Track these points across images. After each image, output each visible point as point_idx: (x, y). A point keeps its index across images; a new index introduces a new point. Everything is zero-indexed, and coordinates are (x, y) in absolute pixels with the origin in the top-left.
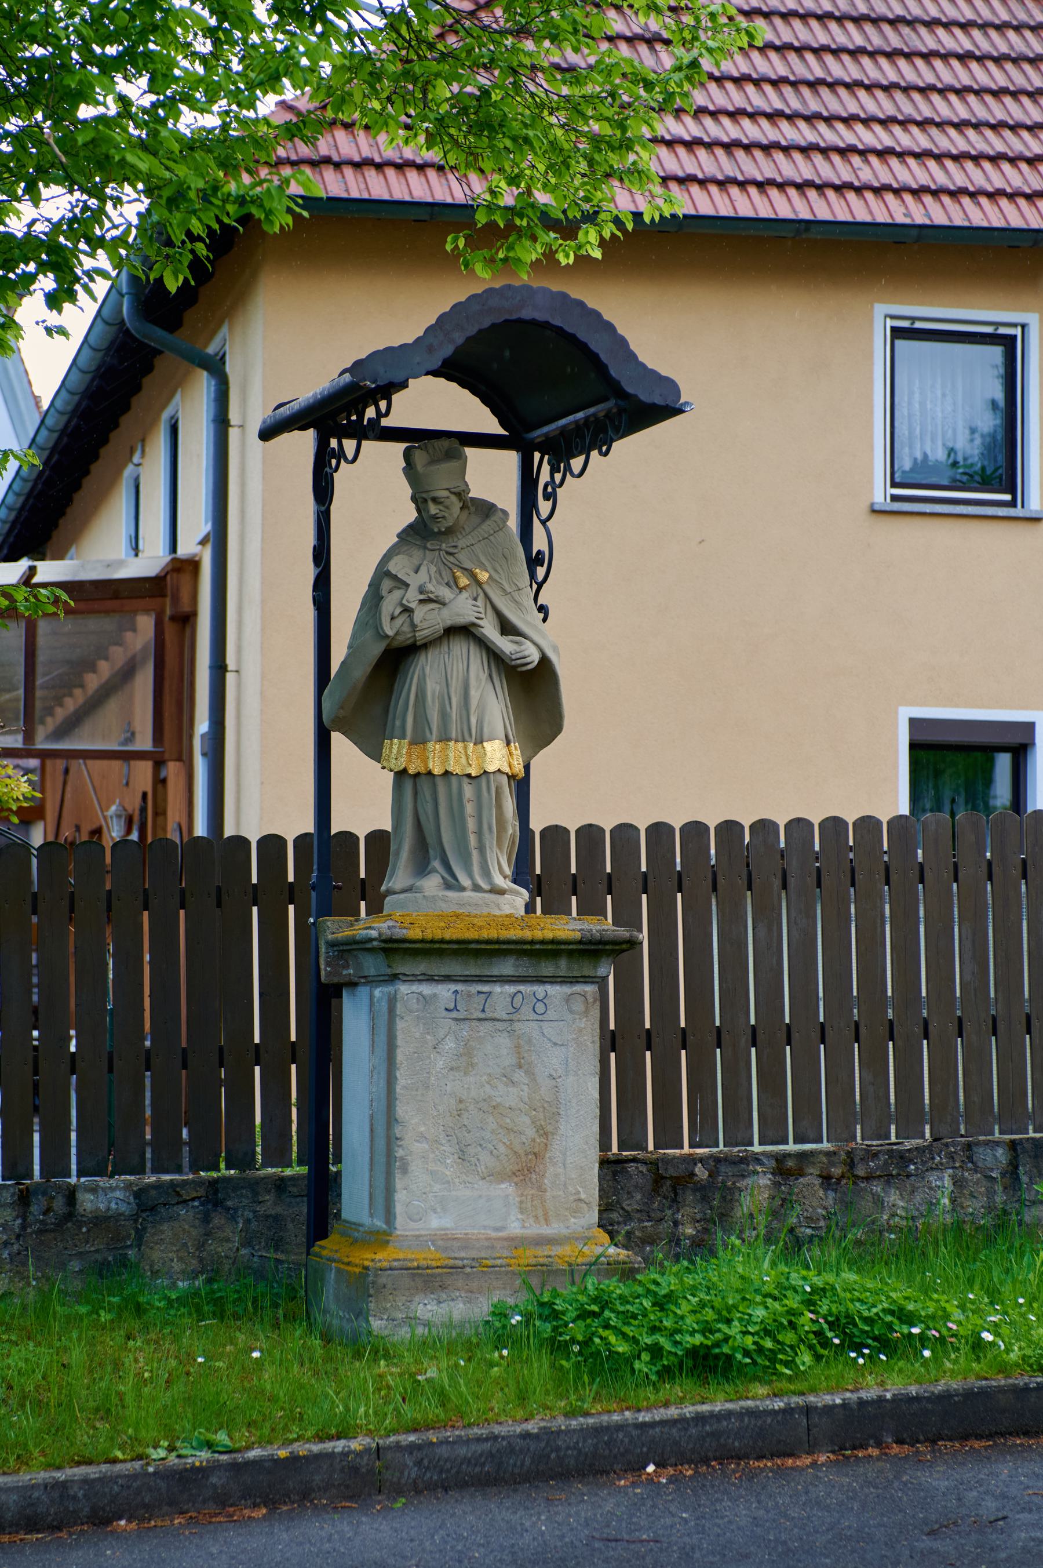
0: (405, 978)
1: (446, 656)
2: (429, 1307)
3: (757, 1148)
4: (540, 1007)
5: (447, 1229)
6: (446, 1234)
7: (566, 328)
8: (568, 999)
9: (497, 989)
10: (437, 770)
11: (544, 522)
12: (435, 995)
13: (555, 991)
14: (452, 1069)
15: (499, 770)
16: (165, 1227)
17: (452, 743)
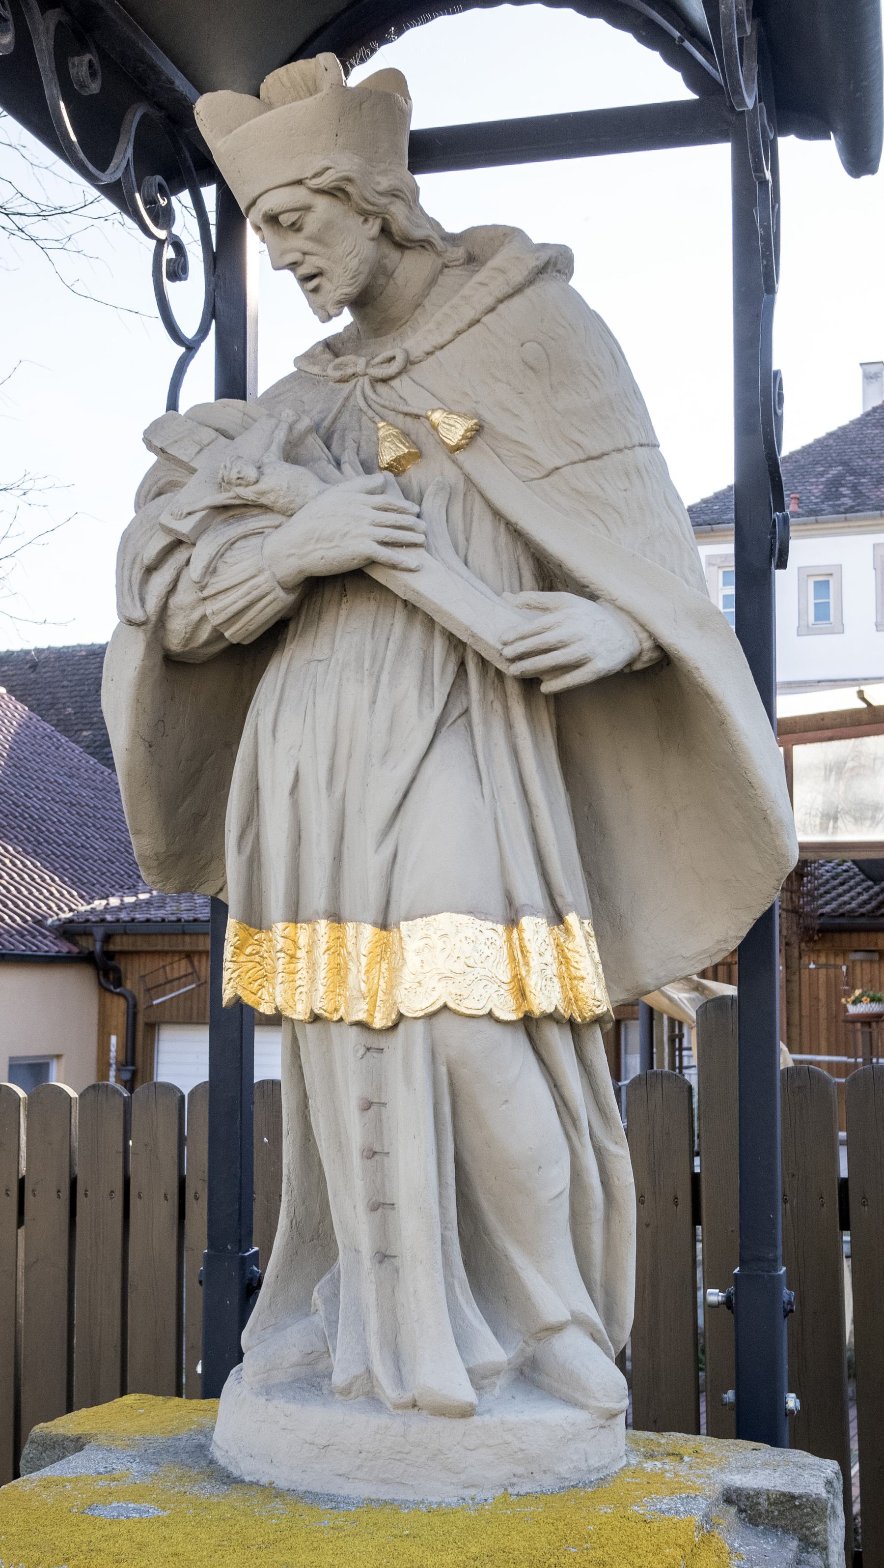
10: (300, 1012)
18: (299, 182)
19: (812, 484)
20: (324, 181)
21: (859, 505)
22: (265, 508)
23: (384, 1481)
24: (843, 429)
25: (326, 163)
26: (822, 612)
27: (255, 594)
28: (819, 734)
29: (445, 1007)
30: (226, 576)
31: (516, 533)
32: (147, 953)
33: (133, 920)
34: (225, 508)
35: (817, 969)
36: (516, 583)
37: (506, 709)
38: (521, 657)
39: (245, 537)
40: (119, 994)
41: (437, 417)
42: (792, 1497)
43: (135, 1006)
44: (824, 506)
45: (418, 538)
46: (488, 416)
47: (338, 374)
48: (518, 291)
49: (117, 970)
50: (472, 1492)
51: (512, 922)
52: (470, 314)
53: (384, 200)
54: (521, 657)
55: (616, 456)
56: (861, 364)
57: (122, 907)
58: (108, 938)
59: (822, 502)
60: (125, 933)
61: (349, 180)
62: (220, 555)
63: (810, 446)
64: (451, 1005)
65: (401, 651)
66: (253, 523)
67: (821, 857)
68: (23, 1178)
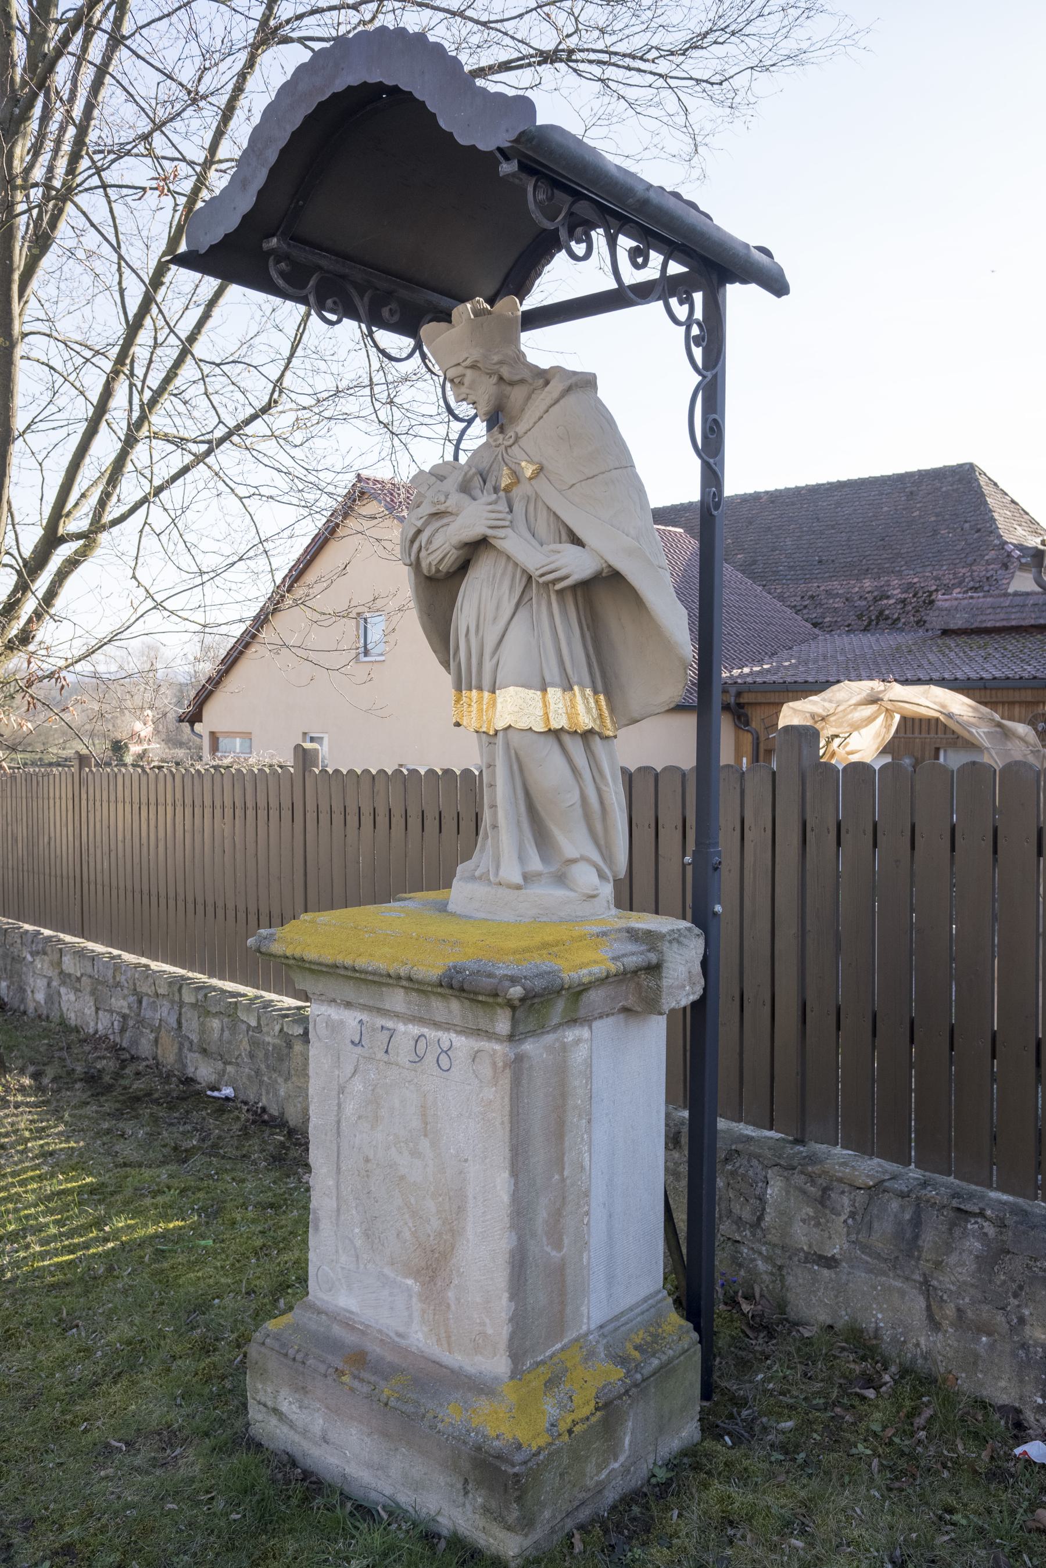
5: (352, 1312)
9: (401, 1027)
18: (459, 364)
29: (510, 726)
30: (437, 542)
32: (764, 703)
33: (755, 682)
34: (437, 514)
36: (557, 539)
40: (748, 731)
41: (523, 464)
42: (651, 931)
43: (758, 738)
45: (507, 523)
46: (545, 462)
48: (557, 401)
49: (746, 716)
51: (544, 690)
52: (538, 414)
53: (497, 367)
55: (601, 476)
57: (751, 673)
58: (739, 694)
60: (750, 691)
61: (476, 361)
62: (433, 535)
65: (503, 574)
66: (445, 521)
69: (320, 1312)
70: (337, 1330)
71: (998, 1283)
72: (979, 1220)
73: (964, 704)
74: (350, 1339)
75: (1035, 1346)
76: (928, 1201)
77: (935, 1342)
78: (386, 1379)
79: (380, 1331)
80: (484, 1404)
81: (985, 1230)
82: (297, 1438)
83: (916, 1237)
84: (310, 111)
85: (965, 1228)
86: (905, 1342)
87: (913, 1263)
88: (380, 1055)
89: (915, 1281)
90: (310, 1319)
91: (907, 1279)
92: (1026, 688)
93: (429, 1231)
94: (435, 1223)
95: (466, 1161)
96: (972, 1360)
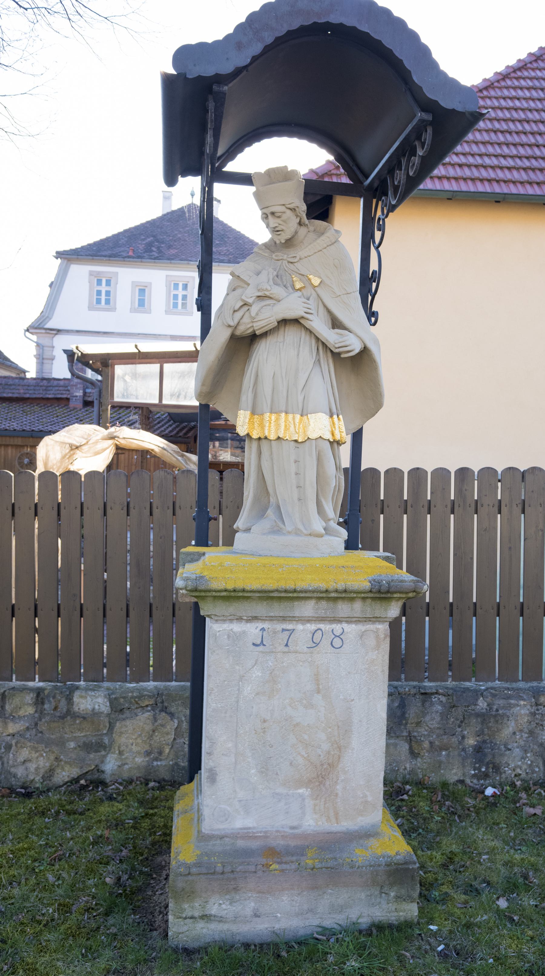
0: (216, 618)
1: (281, 344)
2: (224, 906)
3: (521, 685)
4: (337, 642)
5: (250, 828)
6: (248, 832)
7: (372, 34)
8: (362, 635)
9: (300, 627)
10: (272, 437)
11: (377, 248)
12: (244, 632)
13: (351, 629)
14: (257, 694)
15: (320, 437)
16: (128, 722)
17: (283, 415)
18: (284, 205)
19: (139, 244)
20: (291, 206)
21: (160, 256)
22: (271, 298)
23: (303, 553)
24: (154, 221)
25: (293, 201)
26: (142, 303)
27: (269, 322)
28: (175, 359)
29: (320, 437)
31: (329, 312)
35: (150, 458)
37: (328, 360)
38: (339, 348)
39: (265, 306)
44: (145, 255)
47: (277, 258)
50: (323, 555)
54: (339, 348)
55: (353, 294)
56: (163, 191)
59: (144, 253)
63: (138, 226)
64: (322, 436)
67: (162, 411)
68: (37, 503)
69: (222, 838)
70: (241, 843)
71: (451, 723)
72: (436, 696)
73: (161, 442)
74: (254, 844)
75: (468, 748)
76: (405, 694)
77: (416, 764)
78: (303, 855)
79: (277, 831)
80: (373, 843)
81: (441, 700)
82: (225, 927)
83: (404, 713)
84: (306, 24)
85: (432, 701)
86: (398, 770)
87: (403, 727)
88: (282, 648)
89: (403, 736)
90: (214, 845)
91: (398, 737)
92: (18, 437)
93: (320, 753)
94: (326, 746)
95: (353, 700)
96: (438, 766)
